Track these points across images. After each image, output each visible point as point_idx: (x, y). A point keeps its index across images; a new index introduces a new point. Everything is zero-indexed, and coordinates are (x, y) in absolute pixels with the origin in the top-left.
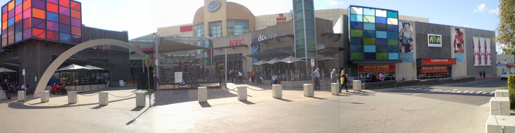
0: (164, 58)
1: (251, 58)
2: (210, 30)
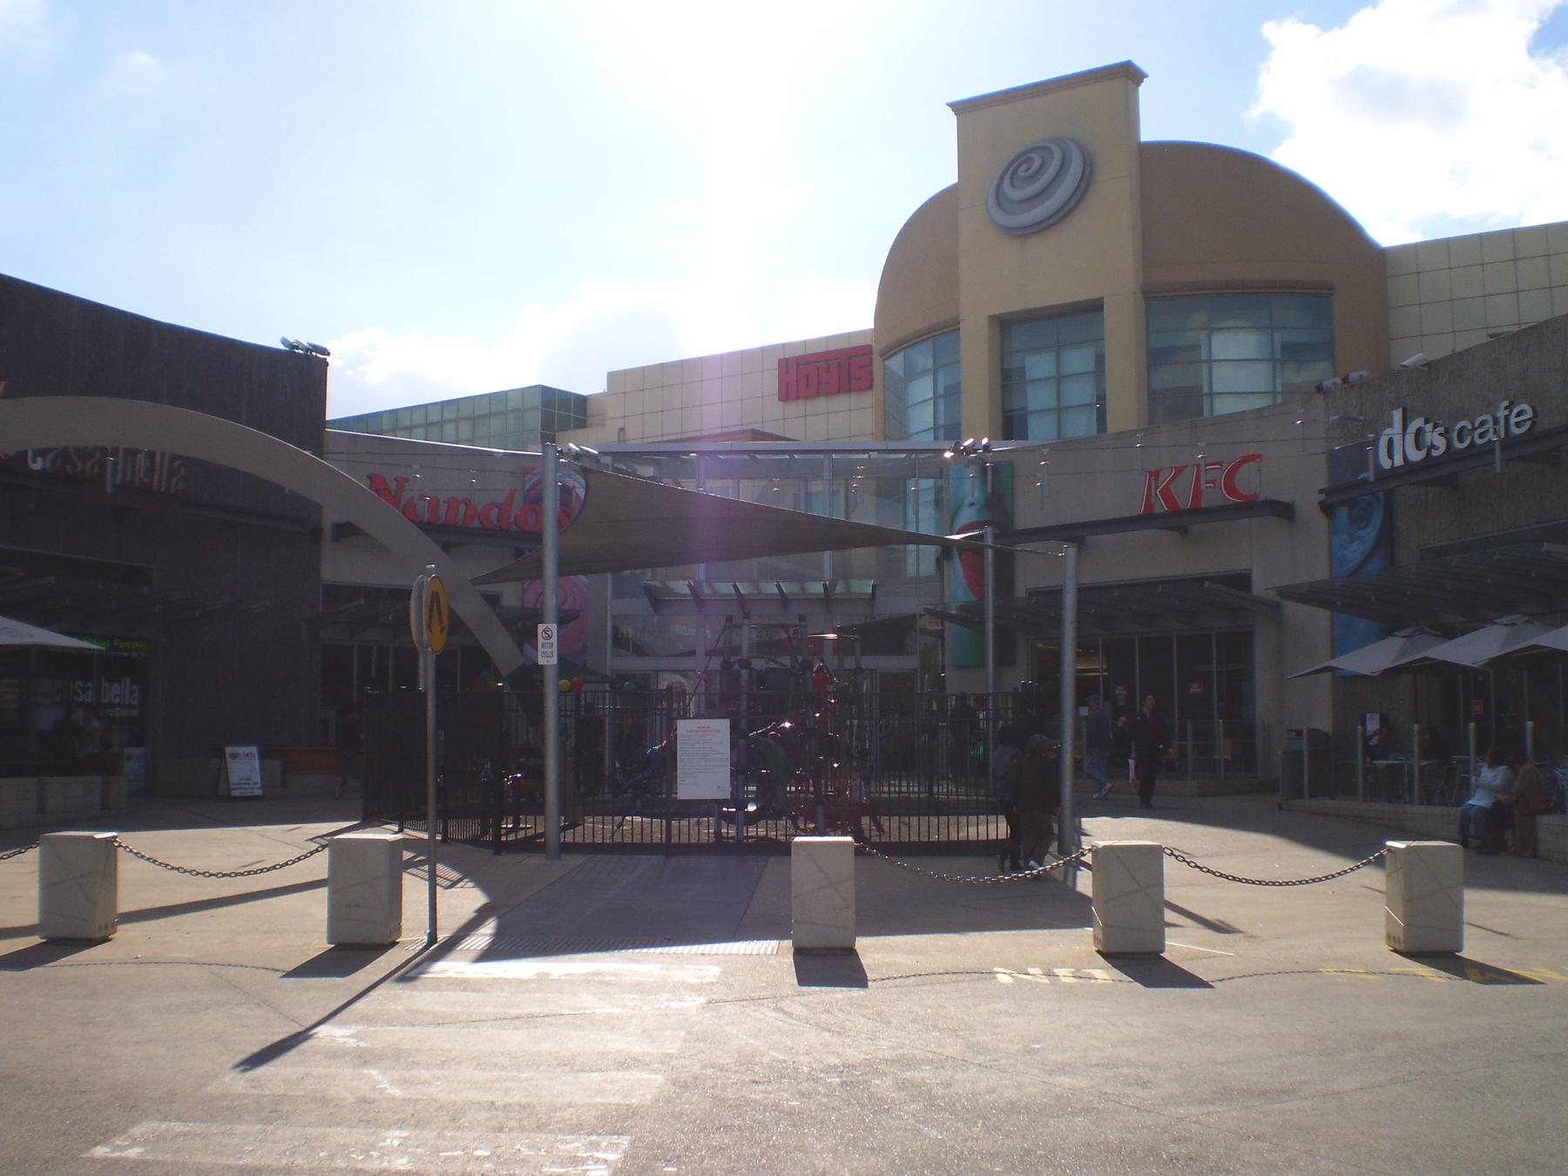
0: (640, 605)
1: (1323, 614)
2: (1009, 379)
